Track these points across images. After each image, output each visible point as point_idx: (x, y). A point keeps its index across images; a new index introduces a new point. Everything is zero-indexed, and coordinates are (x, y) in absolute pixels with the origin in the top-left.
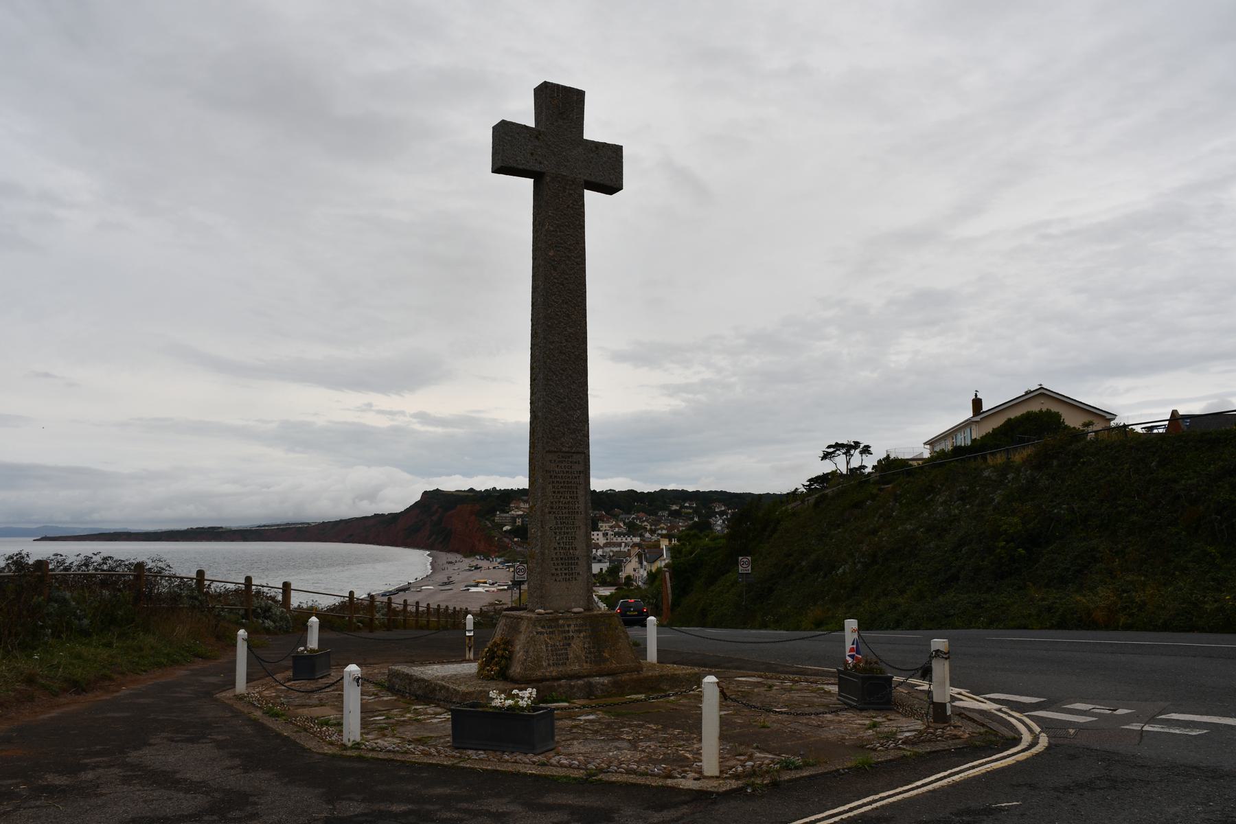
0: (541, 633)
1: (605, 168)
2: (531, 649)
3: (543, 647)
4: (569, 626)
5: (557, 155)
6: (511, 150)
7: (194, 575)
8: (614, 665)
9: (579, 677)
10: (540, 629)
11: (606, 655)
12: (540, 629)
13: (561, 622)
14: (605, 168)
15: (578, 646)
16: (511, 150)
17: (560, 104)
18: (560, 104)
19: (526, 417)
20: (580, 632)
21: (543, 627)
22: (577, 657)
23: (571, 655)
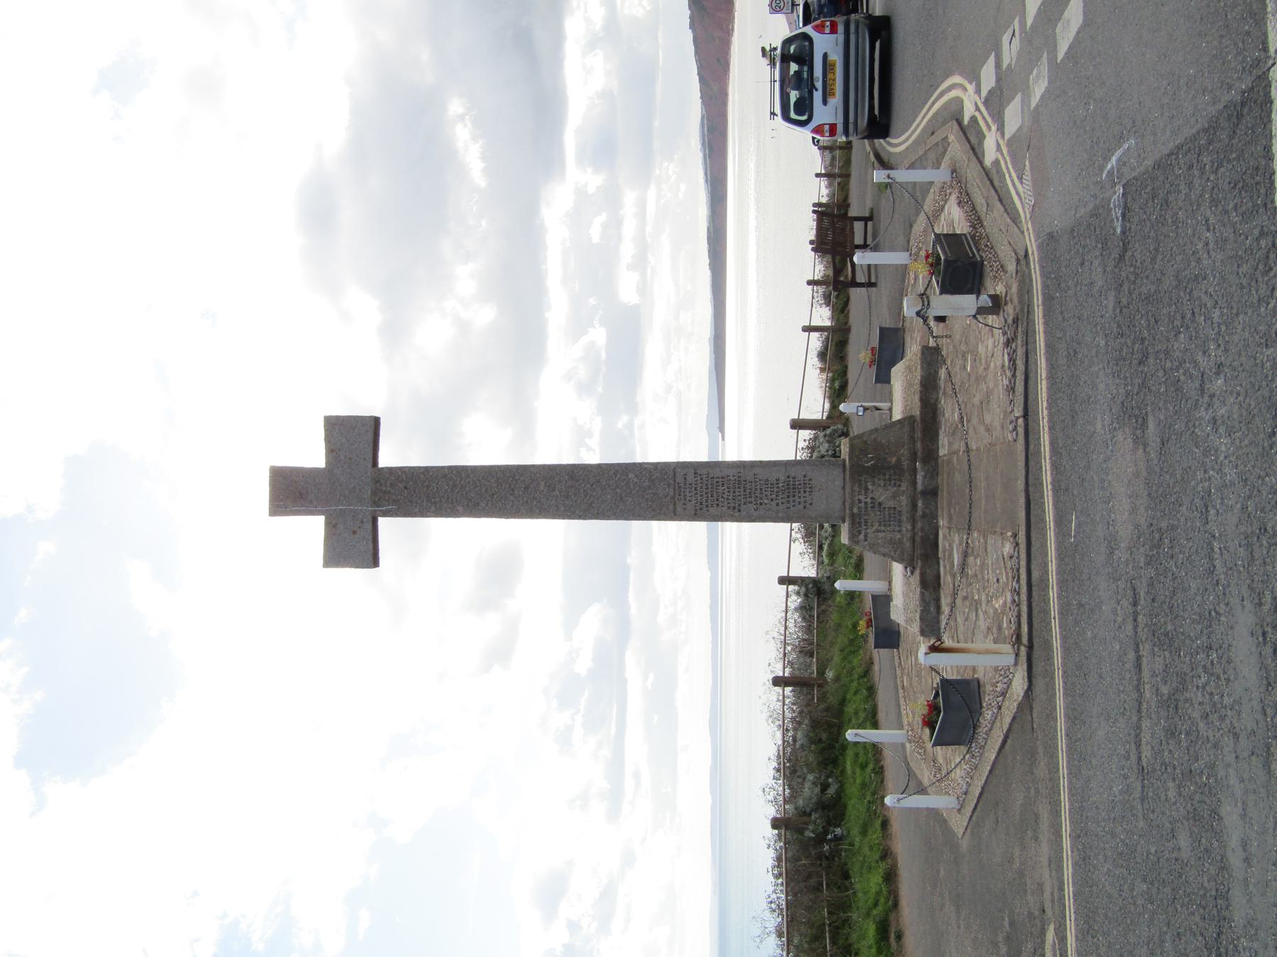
0: (866, 536)
1: (354, 436)
2: (882, 549)
3: (880, 535)
4: (860, 501)
5: (355, 492)
6: (353, 546)
7: (779, 689)
8: (904, 452)
9: (914, 506)
10: (862, 537)
11: (894, 460)
12: (862, 537)
13: (855, 510)
14: (354, 436)
15: (882, 494)
16: (353, 546)
17: (291, 491)
18: (291, 491)
19: (653, 458)
20: (867, 489)
21: (860, 532)
22: (894, 496)
23: (891, 504)
